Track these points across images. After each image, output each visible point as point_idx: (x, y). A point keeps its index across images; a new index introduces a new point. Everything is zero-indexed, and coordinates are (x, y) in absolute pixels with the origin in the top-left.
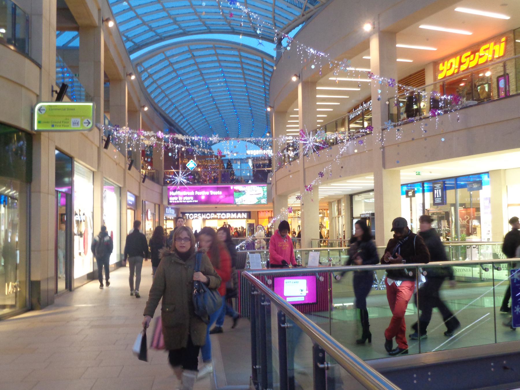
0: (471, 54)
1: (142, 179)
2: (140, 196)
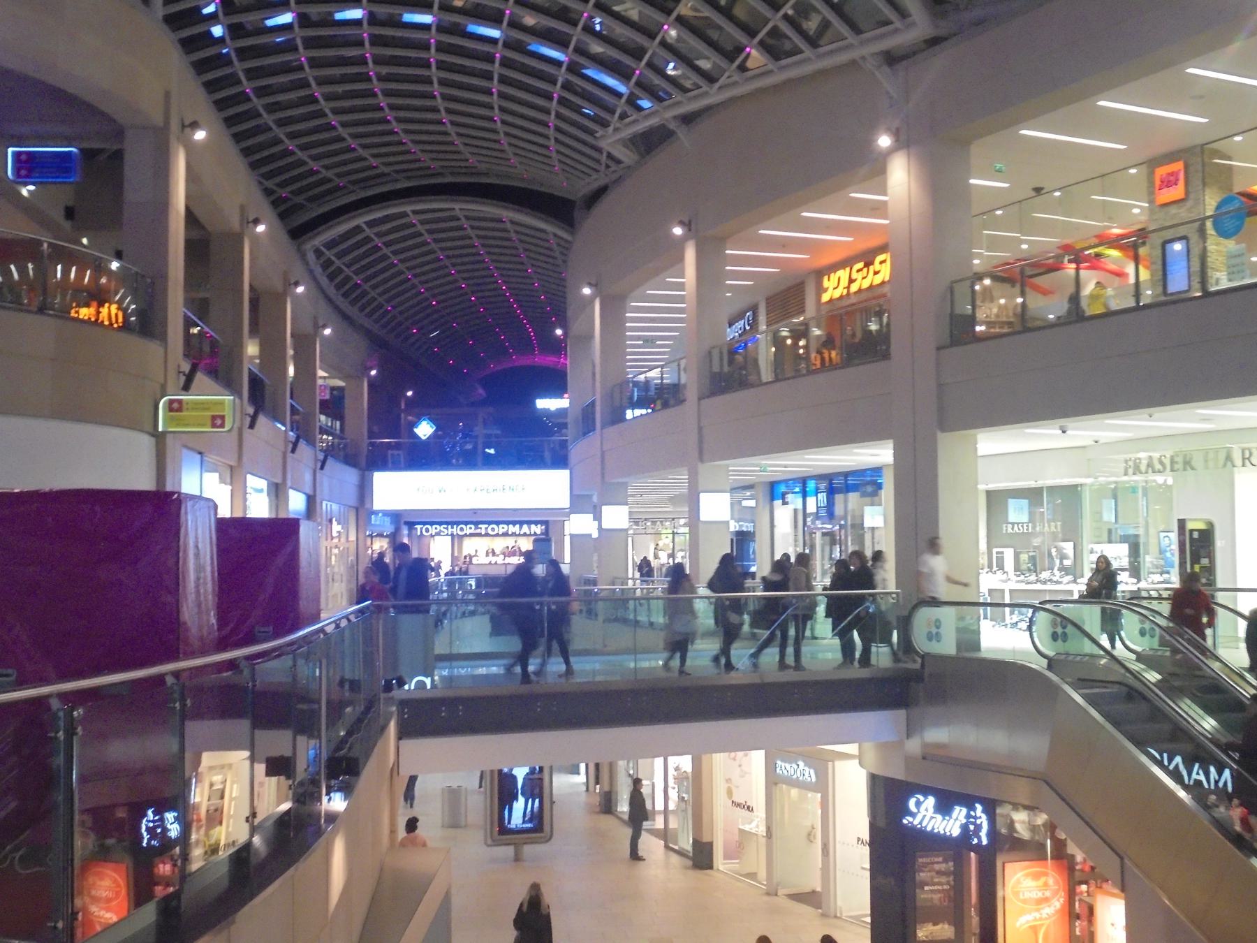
1: (248, 420)
2: (315, 496)
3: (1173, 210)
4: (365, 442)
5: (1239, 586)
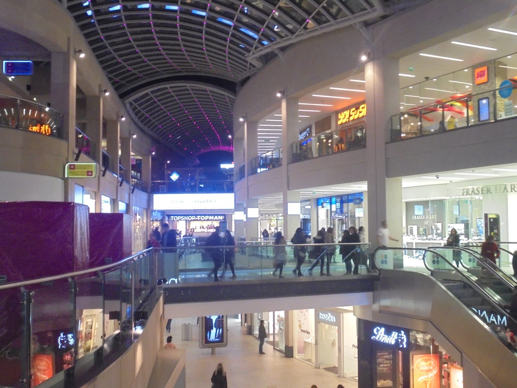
2: (129, 204)
3: (483, 86)
4: (150, 182)
5: (510, 241)
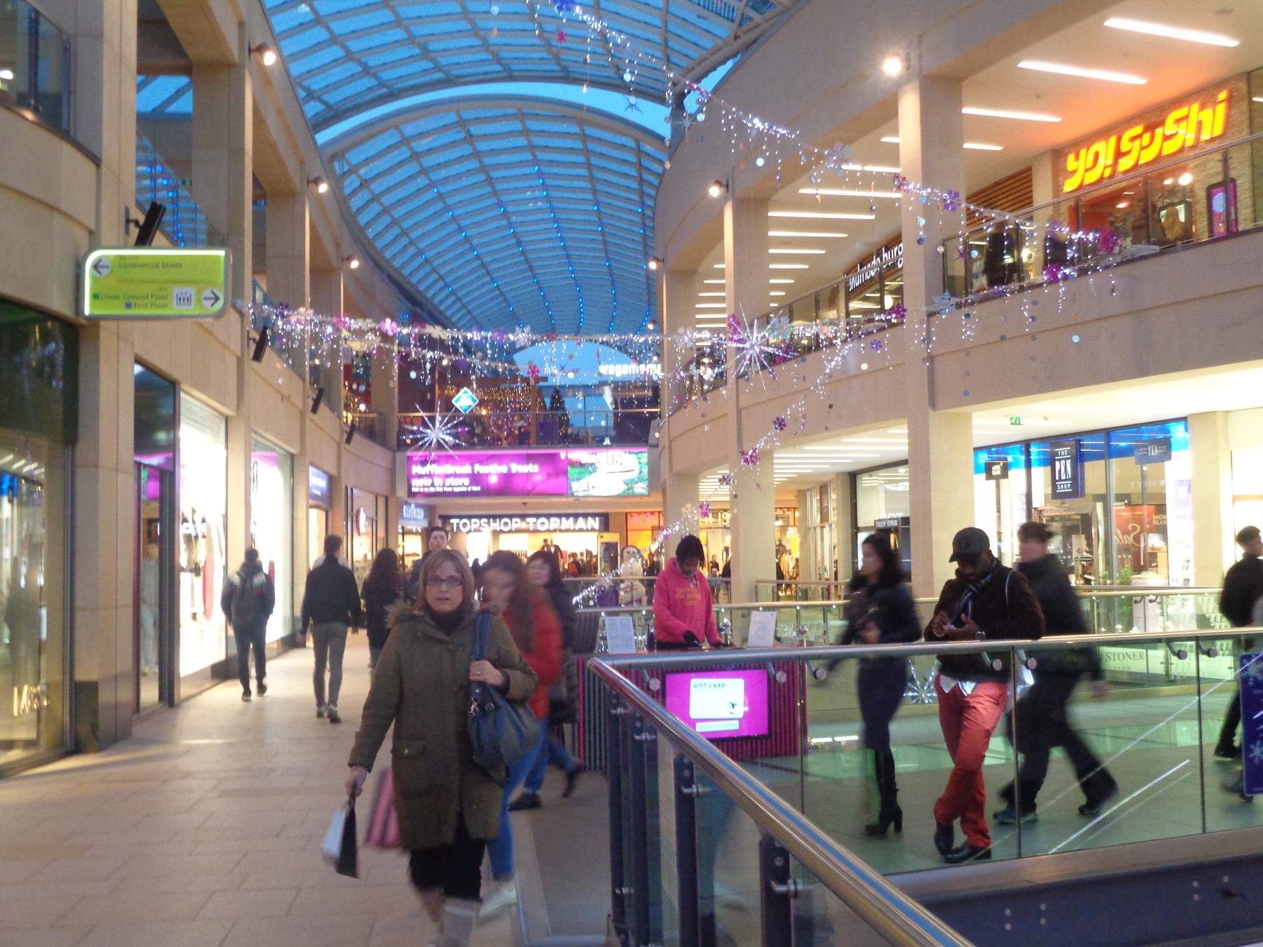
0: (1145, 131)
2: (339, 477)
